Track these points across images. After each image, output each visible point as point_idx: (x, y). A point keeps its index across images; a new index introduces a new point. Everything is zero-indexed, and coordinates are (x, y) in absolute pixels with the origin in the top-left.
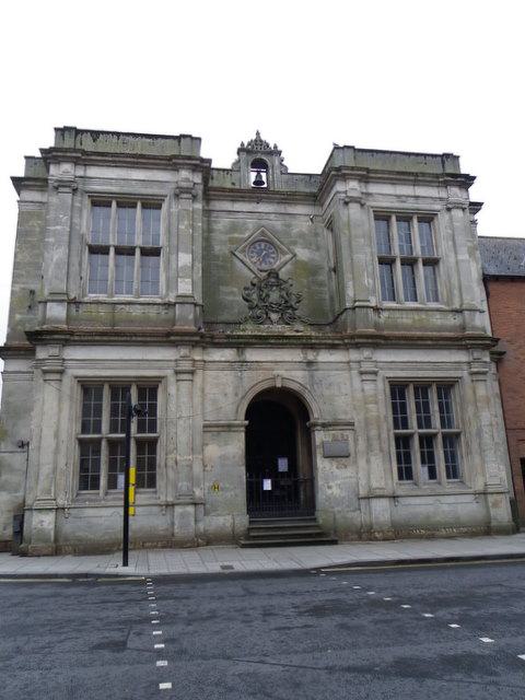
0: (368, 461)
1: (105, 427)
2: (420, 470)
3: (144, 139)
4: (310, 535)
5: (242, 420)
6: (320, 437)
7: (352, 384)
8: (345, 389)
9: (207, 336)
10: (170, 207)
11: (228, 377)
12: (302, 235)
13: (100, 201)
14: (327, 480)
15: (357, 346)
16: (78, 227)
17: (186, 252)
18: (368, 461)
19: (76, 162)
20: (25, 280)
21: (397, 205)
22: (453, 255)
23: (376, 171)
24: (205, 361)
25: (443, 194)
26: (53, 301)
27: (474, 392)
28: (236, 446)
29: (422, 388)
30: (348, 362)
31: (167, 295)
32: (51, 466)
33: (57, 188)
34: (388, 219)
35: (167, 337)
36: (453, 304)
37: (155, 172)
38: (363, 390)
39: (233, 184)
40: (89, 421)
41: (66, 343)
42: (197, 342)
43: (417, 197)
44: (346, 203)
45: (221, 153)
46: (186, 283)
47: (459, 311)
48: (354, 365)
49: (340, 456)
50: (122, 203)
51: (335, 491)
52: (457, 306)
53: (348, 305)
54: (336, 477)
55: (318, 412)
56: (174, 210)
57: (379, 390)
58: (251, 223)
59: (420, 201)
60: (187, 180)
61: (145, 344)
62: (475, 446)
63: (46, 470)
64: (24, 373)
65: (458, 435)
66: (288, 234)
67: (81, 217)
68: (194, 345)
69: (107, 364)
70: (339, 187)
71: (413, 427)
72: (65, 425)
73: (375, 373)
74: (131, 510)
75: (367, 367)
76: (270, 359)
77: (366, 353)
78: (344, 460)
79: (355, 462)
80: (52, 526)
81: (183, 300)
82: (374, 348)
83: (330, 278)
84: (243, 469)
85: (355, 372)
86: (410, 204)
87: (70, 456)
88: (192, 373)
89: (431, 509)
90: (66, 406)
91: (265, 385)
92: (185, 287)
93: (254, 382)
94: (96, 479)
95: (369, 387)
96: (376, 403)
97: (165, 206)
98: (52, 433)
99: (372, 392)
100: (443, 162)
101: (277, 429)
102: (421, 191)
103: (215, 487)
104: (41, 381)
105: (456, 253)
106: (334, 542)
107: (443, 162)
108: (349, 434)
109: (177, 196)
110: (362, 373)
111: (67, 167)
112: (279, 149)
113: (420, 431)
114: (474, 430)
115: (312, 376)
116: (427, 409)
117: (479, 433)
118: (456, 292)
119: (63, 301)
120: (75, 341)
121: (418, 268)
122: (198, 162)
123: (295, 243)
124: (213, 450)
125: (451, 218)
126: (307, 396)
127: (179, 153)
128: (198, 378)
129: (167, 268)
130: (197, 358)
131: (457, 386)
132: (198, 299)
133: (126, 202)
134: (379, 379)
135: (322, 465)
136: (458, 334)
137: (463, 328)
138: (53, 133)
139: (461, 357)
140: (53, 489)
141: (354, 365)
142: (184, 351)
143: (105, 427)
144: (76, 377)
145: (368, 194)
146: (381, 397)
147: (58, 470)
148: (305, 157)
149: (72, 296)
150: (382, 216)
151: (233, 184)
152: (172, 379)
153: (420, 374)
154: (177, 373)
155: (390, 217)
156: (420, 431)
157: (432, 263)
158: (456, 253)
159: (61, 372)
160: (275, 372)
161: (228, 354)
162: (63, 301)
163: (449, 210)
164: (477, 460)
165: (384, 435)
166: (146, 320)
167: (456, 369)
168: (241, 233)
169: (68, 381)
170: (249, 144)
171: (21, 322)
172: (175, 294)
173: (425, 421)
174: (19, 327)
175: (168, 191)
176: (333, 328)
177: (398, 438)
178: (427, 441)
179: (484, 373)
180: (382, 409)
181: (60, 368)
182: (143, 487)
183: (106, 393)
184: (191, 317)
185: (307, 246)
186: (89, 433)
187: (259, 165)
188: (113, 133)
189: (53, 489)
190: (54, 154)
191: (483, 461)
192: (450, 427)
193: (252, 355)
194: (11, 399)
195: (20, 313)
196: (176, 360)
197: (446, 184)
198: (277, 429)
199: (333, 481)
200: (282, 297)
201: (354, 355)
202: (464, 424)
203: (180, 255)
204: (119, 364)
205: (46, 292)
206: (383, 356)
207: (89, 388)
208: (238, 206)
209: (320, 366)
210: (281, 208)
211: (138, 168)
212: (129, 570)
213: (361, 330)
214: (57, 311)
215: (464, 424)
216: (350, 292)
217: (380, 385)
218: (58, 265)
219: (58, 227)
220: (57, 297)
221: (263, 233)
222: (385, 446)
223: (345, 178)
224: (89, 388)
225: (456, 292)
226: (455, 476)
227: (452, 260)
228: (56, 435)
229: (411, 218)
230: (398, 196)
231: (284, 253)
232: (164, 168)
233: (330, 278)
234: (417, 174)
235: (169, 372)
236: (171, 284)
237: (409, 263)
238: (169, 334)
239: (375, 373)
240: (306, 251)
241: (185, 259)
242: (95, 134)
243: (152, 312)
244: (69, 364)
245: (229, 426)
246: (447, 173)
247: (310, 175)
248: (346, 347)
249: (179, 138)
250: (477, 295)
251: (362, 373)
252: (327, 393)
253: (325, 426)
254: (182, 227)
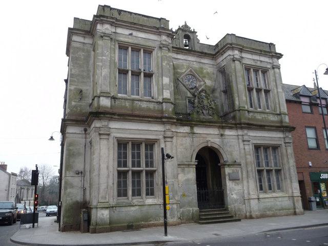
0: (248, 182)
1: (130, 163)
2: (266, 185)
3: (144, 17)
4: (208, 219)
5: (194, 162)
6: (228, 170)
7: (239, 145)
8: (234, 145)
9: (184, 119)
10: (157, 53)
11: (187, 141)
12: (208, 73)
13: (123, 47)
14: (231, 190)
15: (242, 128)
16: (113, 59)
17: (167, 77)
18: (248, 182)
19: (112, 24)
20: (76, 84)
21: (253, 64)
22: (275, 88)
23: (247, 48)
24: (177, 132)
25: (271, 61)
26: (103, 96)
27: (287, 151)
28: (192, 175)
29: (136, 144)
30: (238, 135)
31: (158, 98)
32: (106, 185)
33: (102, 37)
34: (126, 49)
35: (159, 118)
36: (277, 111)
37: (150, 34)
38: (244, 149)
39: (176, 45)
40: (122, 162)
41: (111, 119)
42: (174, 123)
43: (261, 61)
44: (234, 61)
45: (174, 26)
46: (167, 92)
47: (280, 114)
48: (240, 137)
49: (234, 179)
50: (146, 51)
51: (235, 196)
52: (278, 112)
53: (236, 109)
54: (235, 190)
55: (226, 157)
56: (159, 55)
57: (250, 148)
58: (185, 64)
59: (262, 63)
60: (166, 41)
61: (269, 130)
62: (288, 176)
63: (103, 187)
64: (78, 134)
65: (155, 171)
66: (202, 73)
67: (114, 53)
68: (173, 124)
69: (132, 132)
70: (230, 52)
71: (143, 167)
72: (111, 163)
73: (109, 135)
74: (168, 207)
75: (246, 138)
76: (205, 132)
77: (246, 131)
78: (237, 181)
79: (242, 182)
80: (108, 216)
81: (166, 101)
82: (248, 129)
83: (221, 96)
84: (196, 186)
85: (240, 141)
86: (259, 64)
87: (113, 180)
88: (172, 138)
89: (273, 203)
90: (112, 152)
91: (203, 145)
92: (167, 94)
93: (199, 144)
94: (126, 191)
95: (247, 147)
96: (250, 155)
97: (154, 53)
98: (106, 167)
99: (248, 150)
100: (270, 47)
101: (209, 165)
102: (262, 59)
103: (184, 195)
104: (98, 139)
105: (277, 88)
106: (239, 220)
107: (270, 47)
108: (239, 169)
109: (160, 48)
110: (244, 141)
111: (107, 26)
112: (195, 31)
113: (147, 169)
114: (287, 167)
115: (223, 142)
116: (125, 157)
117: (289, 169)
118: (278, 106)
119: (109, 97)
120: (115, 118)
121: (253, 93)
122: (171, 33)
123: (205, 77)
124: (182, 177)
125: (274, 72)
126: (221, 151)
127: (159, 26)
128: (174, 140)
129: (158, 84)
130: (174, 130)
131: (279, 148)
132: (172, 100)
133: (136, 49)
134: (250, 143)
135: (229, 185)
136: (159, 115)
137: (281, 122)
138: (182, 24)
139: (280, 135)
140: (107, 197)
141: (240, 137)
142: (168, 127)
143: (130, 163)
144: (116, 138)
145: (242, 57)
146: (251, 152)
147: (109, 187)
148: (209, 36)
149: (112, 94)
150: (248, 69)
151: (176, 45)
152: (162, 141)
153: (266, 142)
154: (165, 137)
155: (128, 48)
156: (147, 169)
157: (267, 92)
158: (277, 88)
159: (109, 135)
160: (207, 139)
161: (186, 129)
162: (109, 97)
163: (273, 68)
164: (289, 181)
165: (254, 170)
166: (149, 109)
167: (279, 141)
168: (181, 70)
169: (111, 140)
170: (182, 27)
171: (75, 107)
172: (162, 97)
173: (267, 165)
174: (74, 109)
175: (156, 44)
176: (228, 118)
177: (119, 173)
178: (137, 174)
179: (290, 143)
180: (251, 158)
181: (108, 132)
182: (121, 196)
183: (130, 146)
184: (171, 110)
185: (210, 79)
186: (121, 167)
187: (187, 37)
188: (129, 12)
189: (107, 197)
190: (101, 18)
191: (291, 182)
192: (140, 167)
193: (197, 130)
194: (71, 148)
195: (75, 102)
196: (164, 131)
197: (160, 34)
198: (209, 165)
199: (233, 191)
200: (208, 102)
201: (240, 132)
202: (283, 165)
203: (164, 78)
204: (137, 132)
205: (99, 92)
206: (252, 133)
207: (122, 144)
208: (179, 56)
209: (226, 137)
210: (198, 60)
211: (140, 31)
212: (169, 238)
213: (243, 121)
214: (105, 102)
215: (283, 165)
216: (237, 103)
217: (251, 146)
218: (105, 78)
219: (104, 58)
220: (106, 95)
221: (191, 71)
222: (254, 175)
223: (233, 49)
224: (122, 144)
225: (278, 106)
226: (280, 189)
227: (276, 91)
228: (108, 168)
229: (140, 50)
230: (254, 60)
231: (200, 81)
232: (154, 33)
233: (221, 96)
234: (261, 51)
235: (161, 137)
236: (161, 91)
237: (259, 91)
238: (161, 118)
239: (249, 141)
240: (210, 81)
241: (166, 80)
242: (120, 11)
243: (151, 106)
244: (112, 130)
245: (189, 165)
246: (269, 51)
247: (210, 45)
248: (237, 128)
249: (160, 19)
250: (284, 108)
251: (244, 141)
252: (229, 149)
253: (229, 165)
254: (164, 64)
